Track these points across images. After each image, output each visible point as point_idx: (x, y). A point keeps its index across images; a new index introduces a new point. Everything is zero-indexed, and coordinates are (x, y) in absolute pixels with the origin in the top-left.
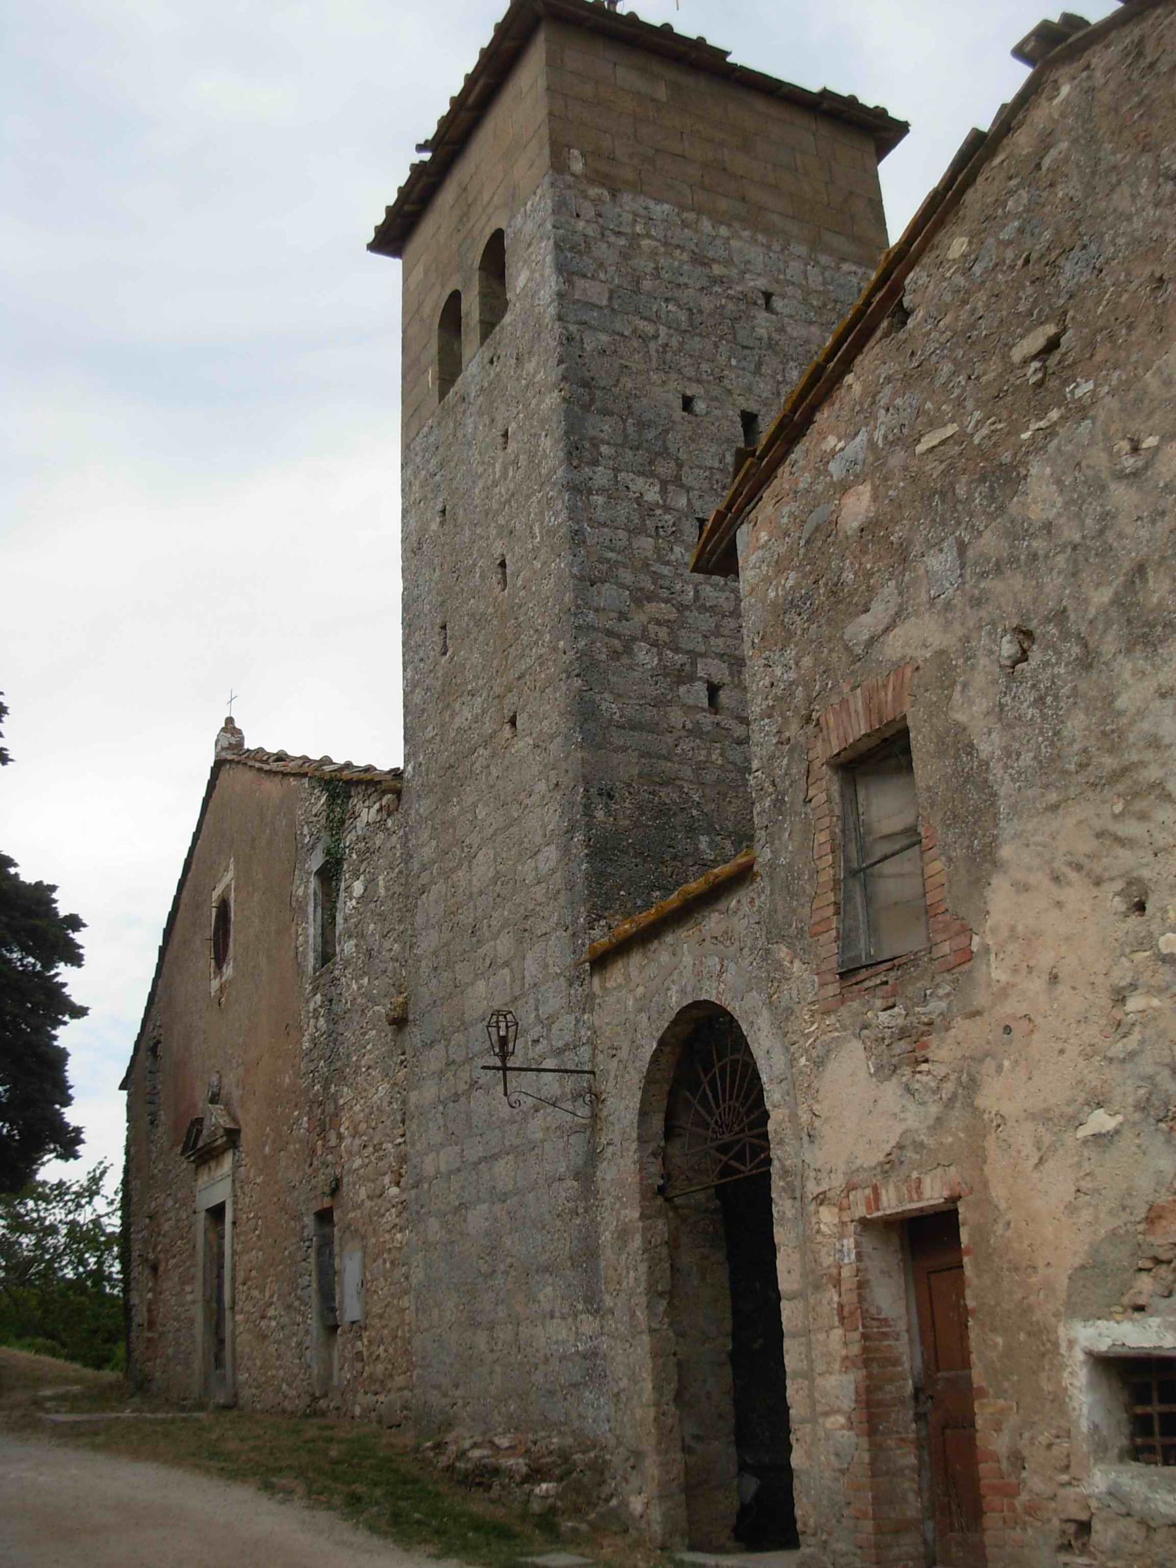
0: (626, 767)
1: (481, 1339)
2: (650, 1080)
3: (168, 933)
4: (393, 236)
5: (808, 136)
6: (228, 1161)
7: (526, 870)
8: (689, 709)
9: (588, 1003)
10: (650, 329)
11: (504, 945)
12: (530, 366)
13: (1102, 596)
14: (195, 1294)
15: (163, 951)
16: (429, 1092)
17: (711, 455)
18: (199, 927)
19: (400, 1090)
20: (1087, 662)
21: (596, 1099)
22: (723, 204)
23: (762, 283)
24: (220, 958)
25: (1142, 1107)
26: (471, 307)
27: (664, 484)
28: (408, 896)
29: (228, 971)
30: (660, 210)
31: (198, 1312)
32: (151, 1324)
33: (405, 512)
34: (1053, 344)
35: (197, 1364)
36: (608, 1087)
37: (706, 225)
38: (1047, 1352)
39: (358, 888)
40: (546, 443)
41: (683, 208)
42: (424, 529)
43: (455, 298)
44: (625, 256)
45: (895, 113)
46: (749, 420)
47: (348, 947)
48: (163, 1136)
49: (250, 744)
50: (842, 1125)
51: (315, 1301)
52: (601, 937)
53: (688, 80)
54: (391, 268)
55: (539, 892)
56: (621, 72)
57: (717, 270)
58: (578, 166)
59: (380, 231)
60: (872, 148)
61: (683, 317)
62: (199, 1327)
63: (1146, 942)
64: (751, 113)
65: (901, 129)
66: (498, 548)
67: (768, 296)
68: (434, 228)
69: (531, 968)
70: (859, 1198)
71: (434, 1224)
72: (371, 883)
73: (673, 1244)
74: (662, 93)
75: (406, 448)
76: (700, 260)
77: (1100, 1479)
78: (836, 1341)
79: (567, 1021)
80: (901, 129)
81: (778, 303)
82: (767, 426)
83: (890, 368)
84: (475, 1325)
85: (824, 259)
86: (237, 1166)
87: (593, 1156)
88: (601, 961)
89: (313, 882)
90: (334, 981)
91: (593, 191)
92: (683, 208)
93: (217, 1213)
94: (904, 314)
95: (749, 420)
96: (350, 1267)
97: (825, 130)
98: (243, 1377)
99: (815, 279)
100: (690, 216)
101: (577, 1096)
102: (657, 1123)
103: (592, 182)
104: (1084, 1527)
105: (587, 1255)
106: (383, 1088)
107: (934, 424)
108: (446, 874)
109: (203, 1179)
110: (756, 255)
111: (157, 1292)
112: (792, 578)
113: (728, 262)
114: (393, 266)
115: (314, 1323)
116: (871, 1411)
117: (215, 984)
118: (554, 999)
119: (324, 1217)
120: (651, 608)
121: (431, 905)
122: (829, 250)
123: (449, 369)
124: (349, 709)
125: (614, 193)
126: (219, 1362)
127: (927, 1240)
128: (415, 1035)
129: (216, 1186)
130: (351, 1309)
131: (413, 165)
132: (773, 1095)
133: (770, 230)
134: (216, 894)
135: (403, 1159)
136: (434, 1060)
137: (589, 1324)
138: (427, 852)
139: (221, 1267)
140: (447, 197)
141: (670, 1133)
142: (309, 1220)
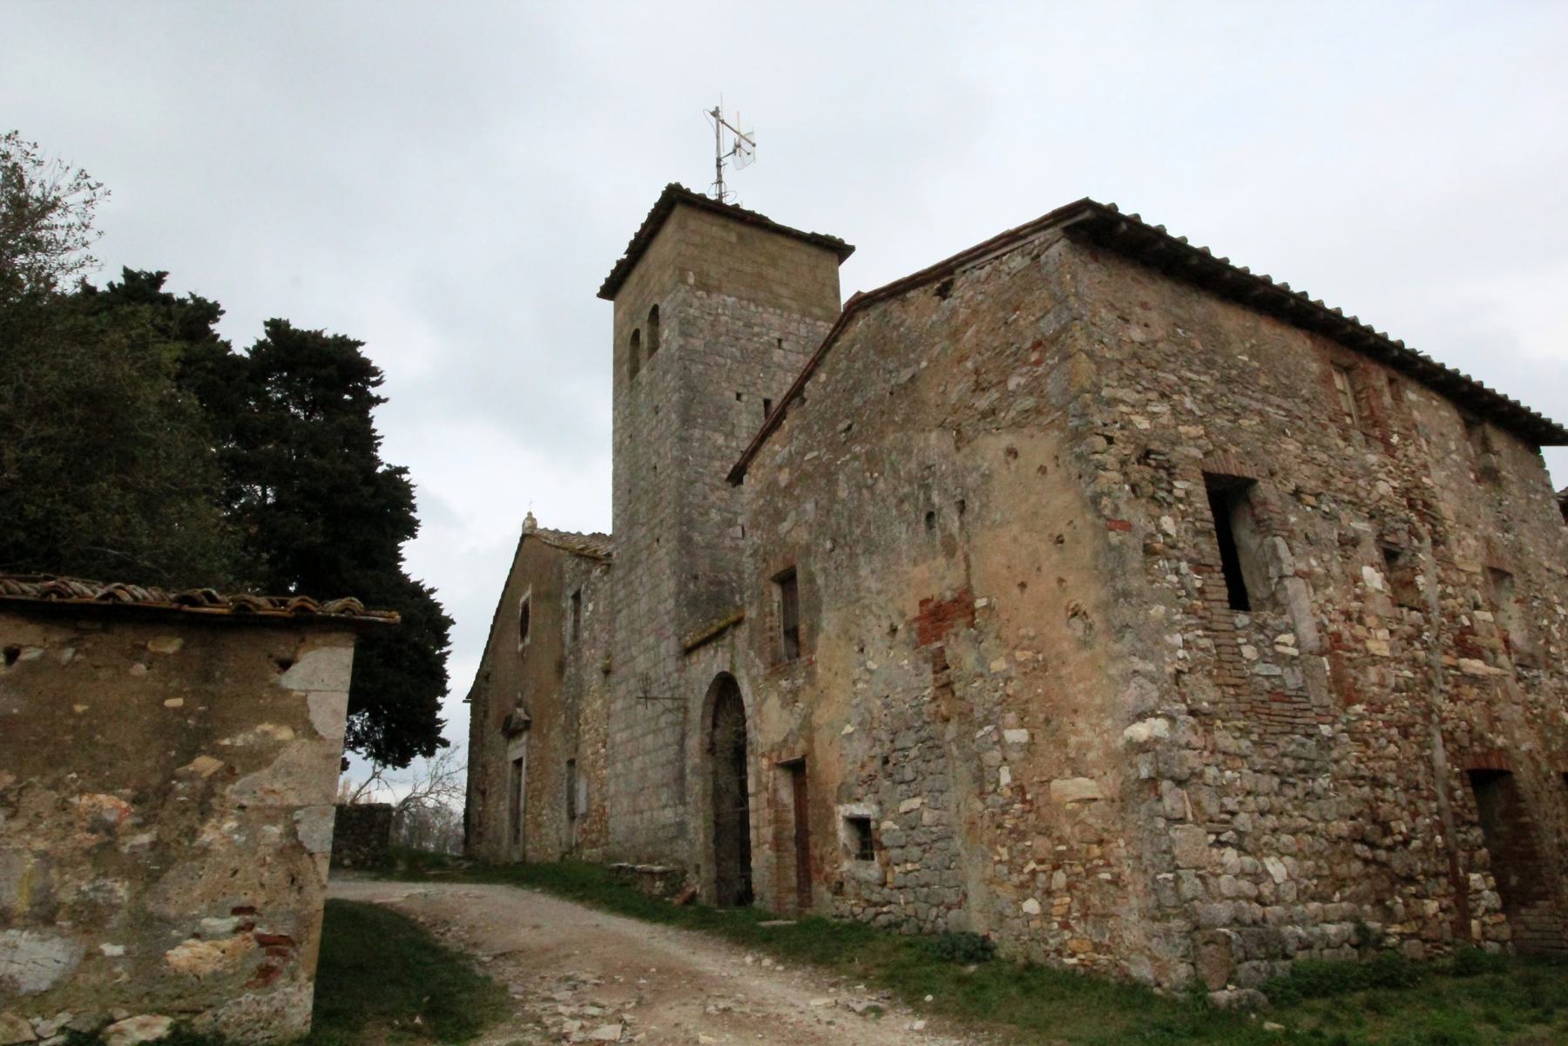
0: (703, 565)
1: (637, 818)
2: (705, 704)
3: (495, 618)
4: (610, 290)
5: (804, 254)
6: (524, 738)
7: (661, 608)
8: (733, 539)
9: (681, 670)
10: (721, 361)
11: (651, 640)
12: (669, 377)
13: (858, 531)
14: (504, 807)
15: (493, 627)
16: (619, 705)
17: (748, 422)
18: (512, 618)
19: (607, 705)
20: (852, 556)
21: (686, 710)
22: (761, 295)
23: (777, 335)
24: (524, 633)
25: (860, 724)
26: (644, 337)
27: (726, 436)
28: (613, 614)
29: (528, 640)
30: (730, 300)
31: (506, 816)
32: (480, 824)
33: (615, 432)
34: (849, 428)
35: (505, 842)
36: (690, 705)
37: (752, 307)
38: (830, 815)
39: (591, 606)
40: (673, 416)
41: (741, 298)
42: (622, 443)
43: (636, 334)
44: (713, 326)
45: (848, 242)
46: (767, 403)
47: (586, 634)
48: (491, 722)
49: (540, 526)
50: (770, 722)
51: (565, 805)
52: (689, 641)
53: (746, 230)
54: (608, 305)
55: (666, 618)
56: (714, 229)
57: (756, 329)
58: (691, 280)
59: (603, 288)
60: (836, 258)
61: (738, 354)
62: (507, 824)
63: (863, 664)
64: (773, 245)
65: (851, 249)
66: (654, 460)
67: (780, 341)
68: (629, 288)
69: (662, 651)
70: (774, 755)
71: (619, 765)
72: (596, 605)
73: (715, 773)
74: (733, 238)
75: (615, 400)
76: (748, 325)
77: (847, 865)
78: (768, 814)
79: (676, 675)
80: (851, 249)
81: (784, 345)
82: (775, 404)
83: (797, 422)
84: (635, 812)
85: (808, 320)
86: (529, 738)
87: (683, 736)
88: (688, 651)
89: (570, 602)
90: (579, 650)
91: (699, 293)
92: (741, 298)
93: (518, 763)
94: (804, 400)
95: (767, 403)
96: (582, 786)
97: (814, 251)
98: (529, 847)
99: (803, 331)
100: (744, 303)
101: (678, 709)
102: (709, 722)
103: (699, 289)
104: (842, 884)
105: (681, 778)
106: (599, 702)
107: (811, 449)
108: (629, 606)
109: (512, 746)
110: (775, 320)
111: (485, 806)
112: (761, 502)
113: (762, 325)
114: (610, 304)
115: (565, 816)
116: (778, 843)
117: (520, 647)
118: (671, 666)
119: (571, 763)
120: (718, 493)
121: (622, 618)
122: (811, 315)
123: (634, 371)
124: (585, 505)
125: (709, 292)
126: (516, 840)
127: (797, 769)
128: (613, 679)
129: (517, 749)
130: (581, 807)
131: (415, 537)
132: (749, 711)
133: (782, 307)
134: (522, 600)
135: (607, 735)
136: (622, 689)
137: (681, 809)
138: (622, 594)
139: (519, 791)
140: (634, 278)
141: (715, 726)
142: (564, 765)
